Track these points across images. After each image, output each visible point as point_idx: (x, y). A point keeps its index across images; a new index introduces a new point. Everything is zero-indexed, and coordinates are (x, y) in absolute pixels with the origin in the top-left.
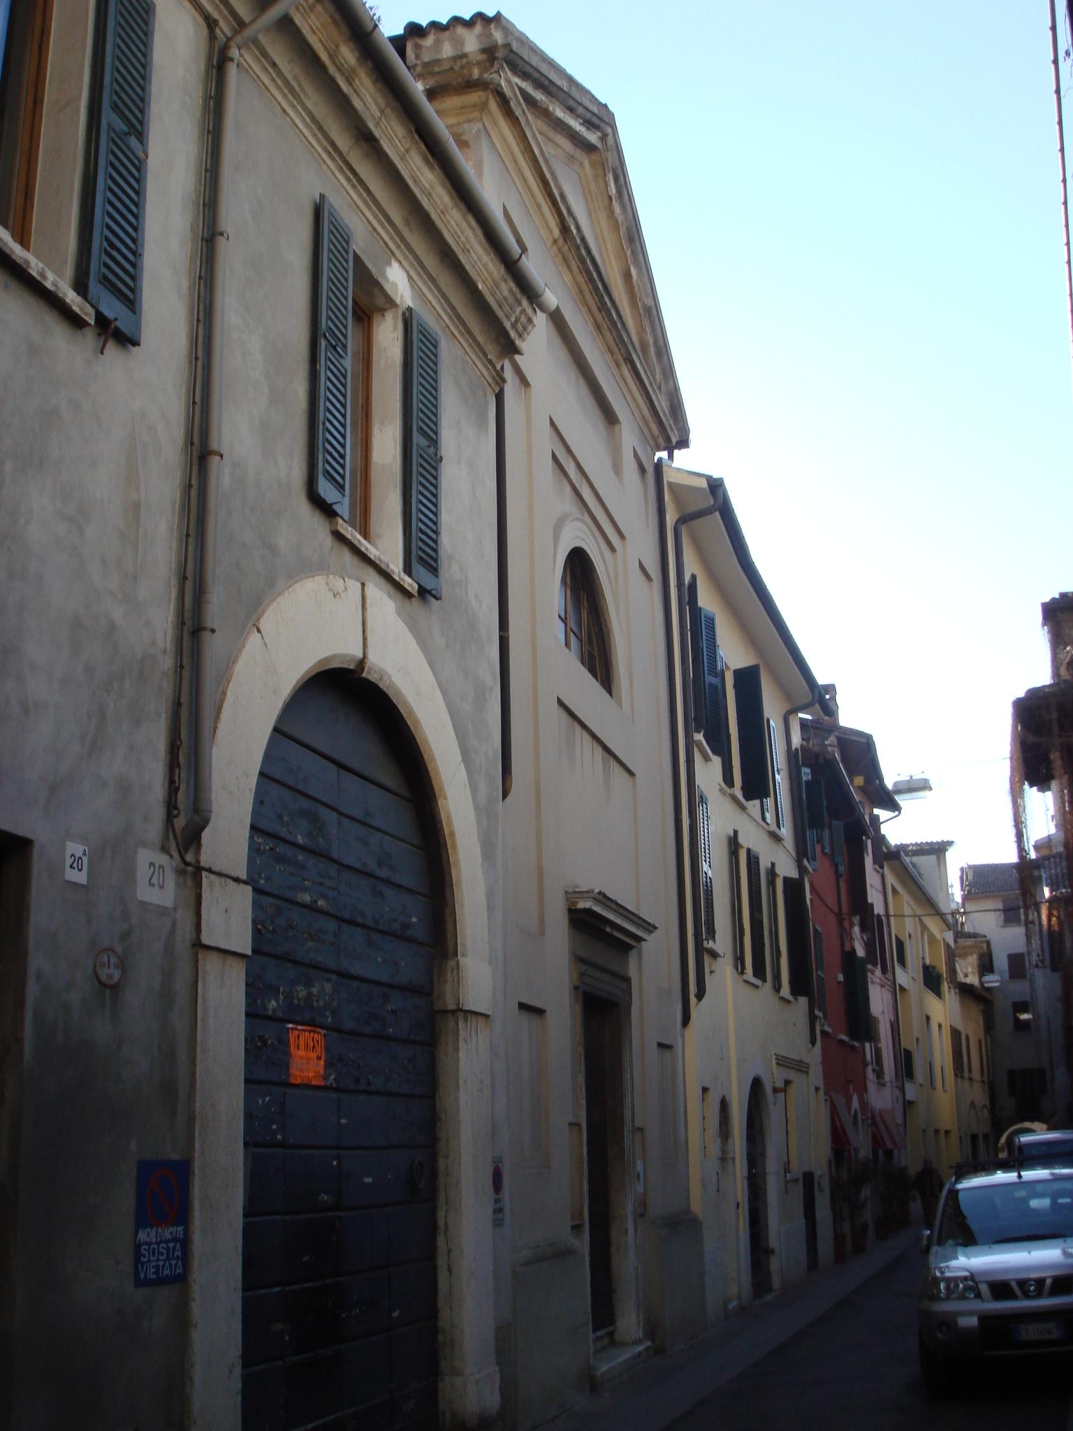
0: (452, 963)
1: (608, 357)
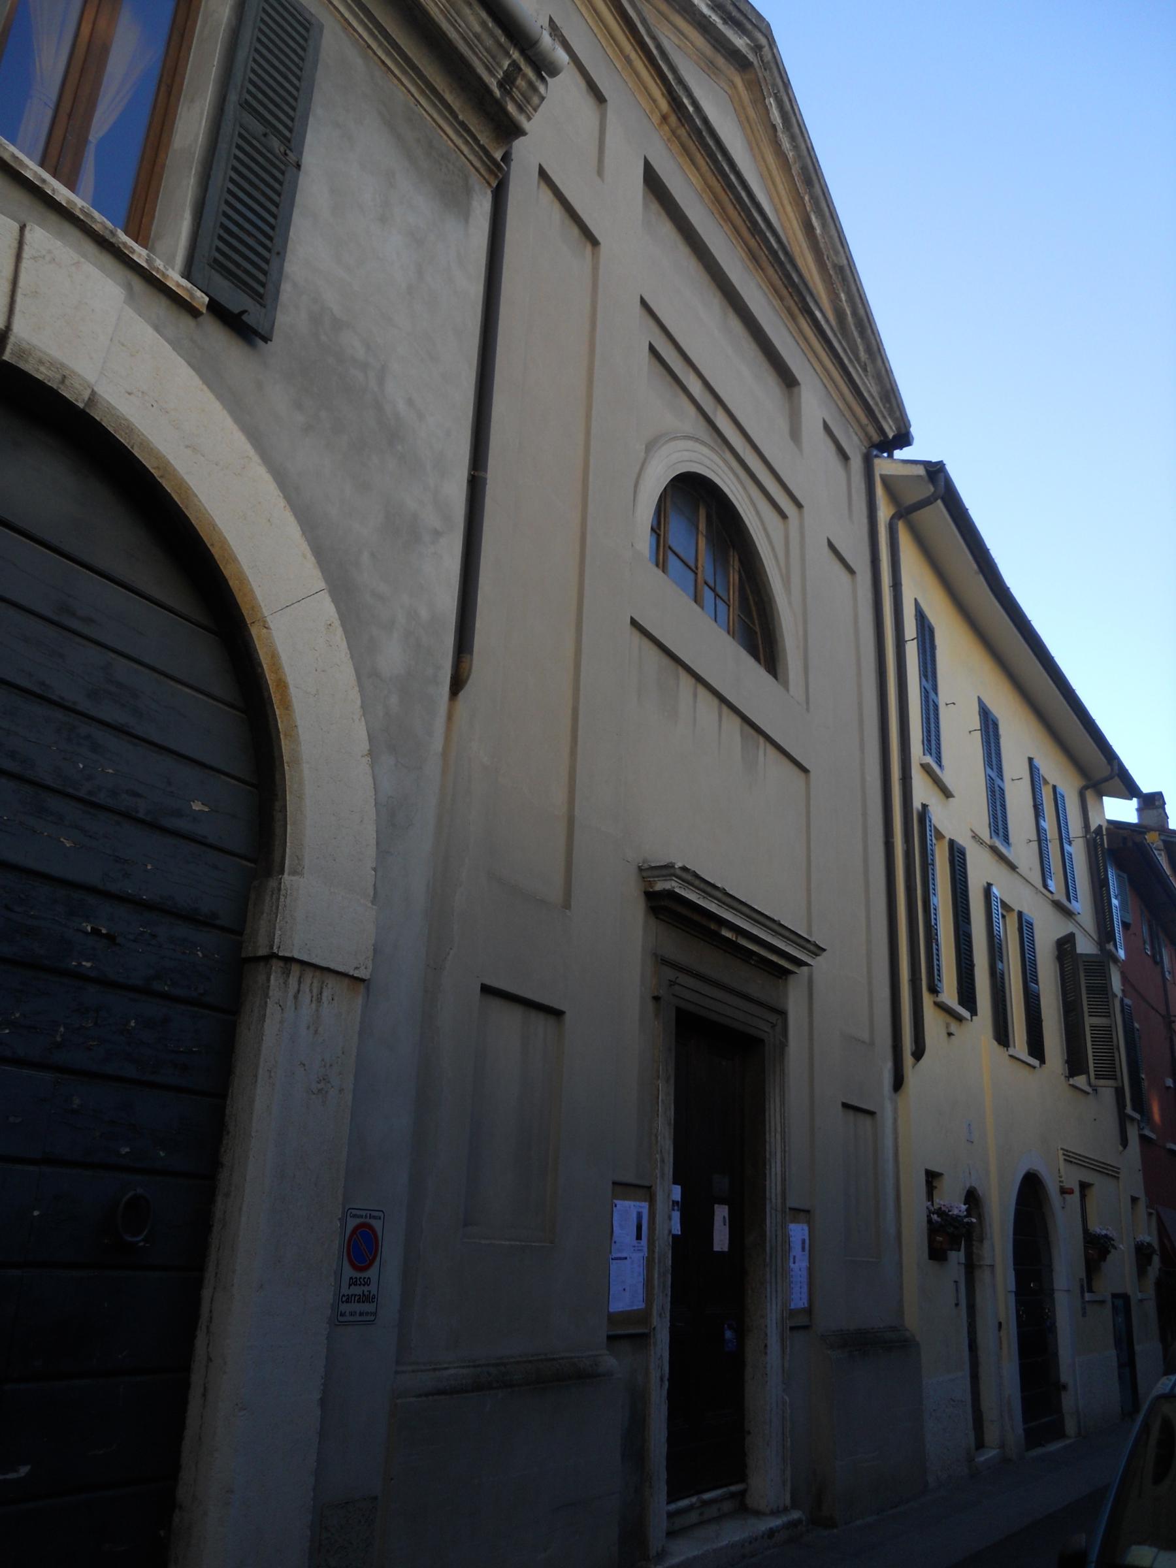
0: (272, 883)
1: (776, 303)
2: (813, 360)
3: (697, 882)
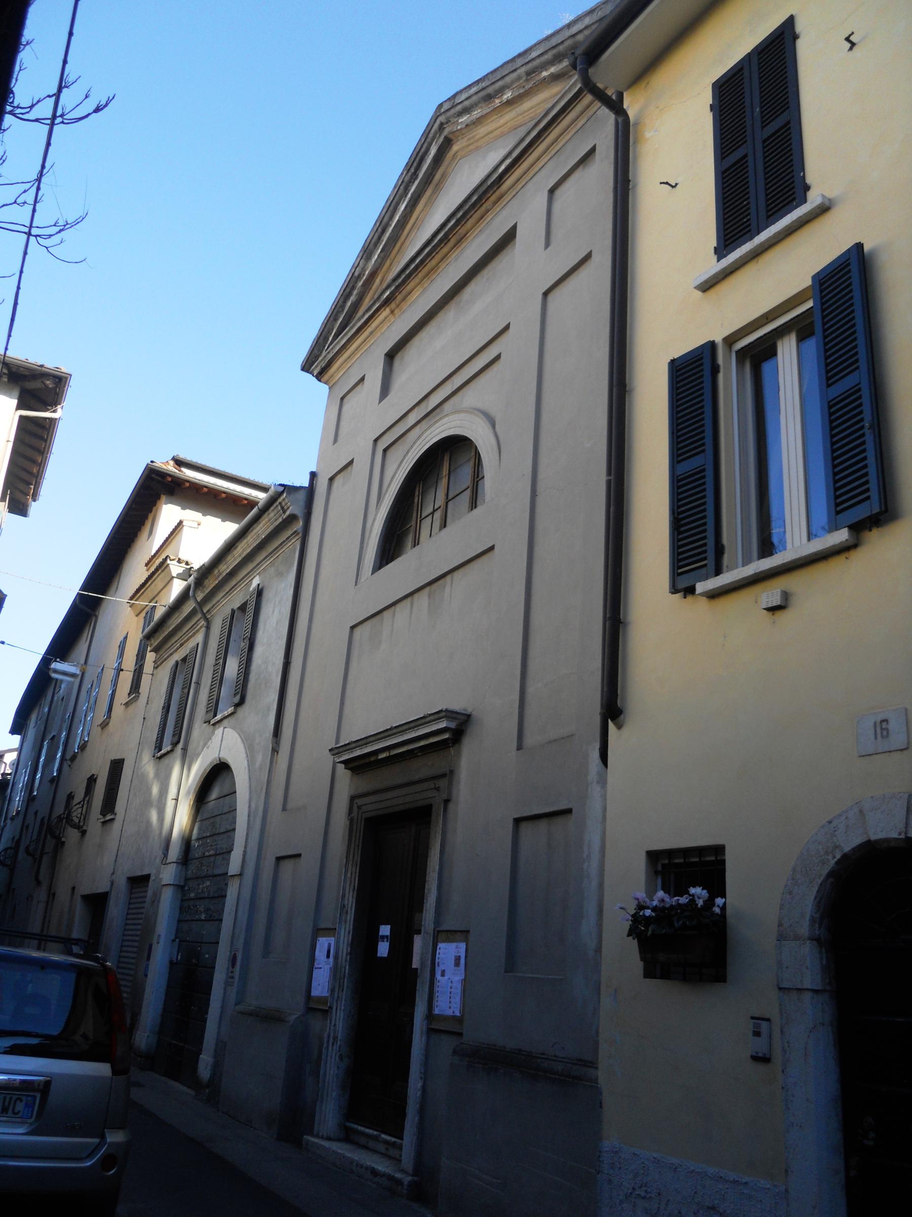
2: (536, 168)
3: (341, 750)
